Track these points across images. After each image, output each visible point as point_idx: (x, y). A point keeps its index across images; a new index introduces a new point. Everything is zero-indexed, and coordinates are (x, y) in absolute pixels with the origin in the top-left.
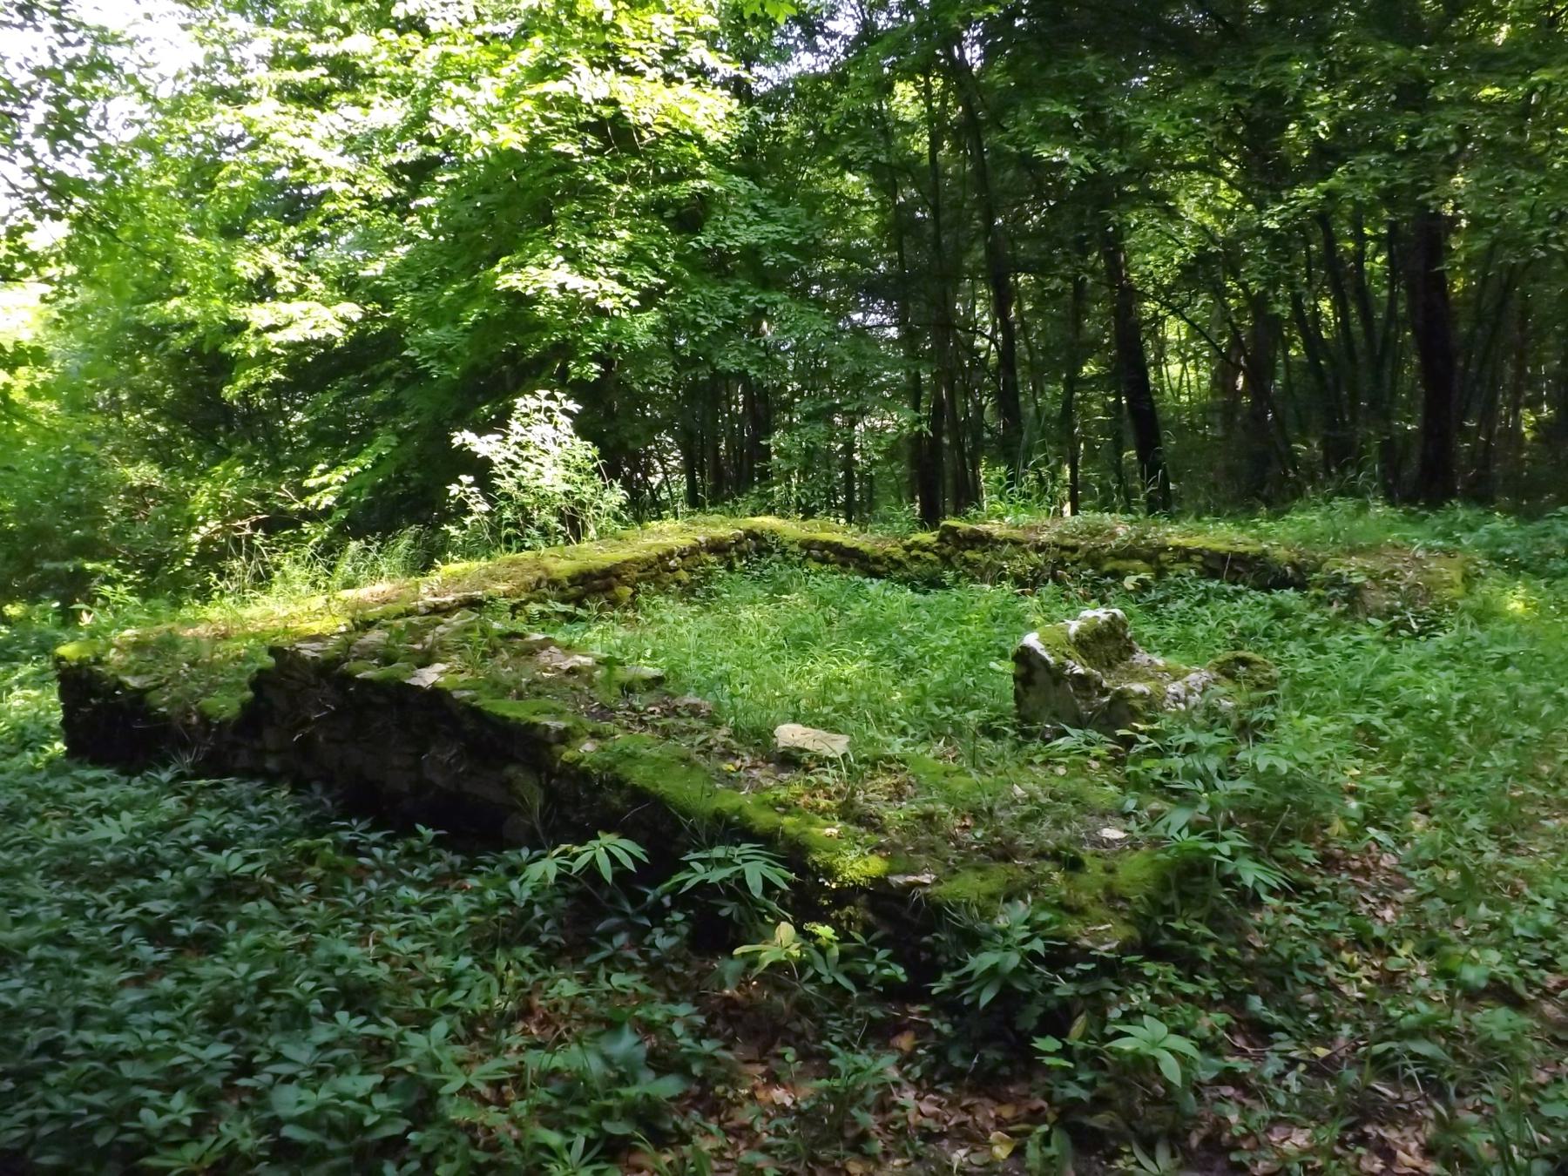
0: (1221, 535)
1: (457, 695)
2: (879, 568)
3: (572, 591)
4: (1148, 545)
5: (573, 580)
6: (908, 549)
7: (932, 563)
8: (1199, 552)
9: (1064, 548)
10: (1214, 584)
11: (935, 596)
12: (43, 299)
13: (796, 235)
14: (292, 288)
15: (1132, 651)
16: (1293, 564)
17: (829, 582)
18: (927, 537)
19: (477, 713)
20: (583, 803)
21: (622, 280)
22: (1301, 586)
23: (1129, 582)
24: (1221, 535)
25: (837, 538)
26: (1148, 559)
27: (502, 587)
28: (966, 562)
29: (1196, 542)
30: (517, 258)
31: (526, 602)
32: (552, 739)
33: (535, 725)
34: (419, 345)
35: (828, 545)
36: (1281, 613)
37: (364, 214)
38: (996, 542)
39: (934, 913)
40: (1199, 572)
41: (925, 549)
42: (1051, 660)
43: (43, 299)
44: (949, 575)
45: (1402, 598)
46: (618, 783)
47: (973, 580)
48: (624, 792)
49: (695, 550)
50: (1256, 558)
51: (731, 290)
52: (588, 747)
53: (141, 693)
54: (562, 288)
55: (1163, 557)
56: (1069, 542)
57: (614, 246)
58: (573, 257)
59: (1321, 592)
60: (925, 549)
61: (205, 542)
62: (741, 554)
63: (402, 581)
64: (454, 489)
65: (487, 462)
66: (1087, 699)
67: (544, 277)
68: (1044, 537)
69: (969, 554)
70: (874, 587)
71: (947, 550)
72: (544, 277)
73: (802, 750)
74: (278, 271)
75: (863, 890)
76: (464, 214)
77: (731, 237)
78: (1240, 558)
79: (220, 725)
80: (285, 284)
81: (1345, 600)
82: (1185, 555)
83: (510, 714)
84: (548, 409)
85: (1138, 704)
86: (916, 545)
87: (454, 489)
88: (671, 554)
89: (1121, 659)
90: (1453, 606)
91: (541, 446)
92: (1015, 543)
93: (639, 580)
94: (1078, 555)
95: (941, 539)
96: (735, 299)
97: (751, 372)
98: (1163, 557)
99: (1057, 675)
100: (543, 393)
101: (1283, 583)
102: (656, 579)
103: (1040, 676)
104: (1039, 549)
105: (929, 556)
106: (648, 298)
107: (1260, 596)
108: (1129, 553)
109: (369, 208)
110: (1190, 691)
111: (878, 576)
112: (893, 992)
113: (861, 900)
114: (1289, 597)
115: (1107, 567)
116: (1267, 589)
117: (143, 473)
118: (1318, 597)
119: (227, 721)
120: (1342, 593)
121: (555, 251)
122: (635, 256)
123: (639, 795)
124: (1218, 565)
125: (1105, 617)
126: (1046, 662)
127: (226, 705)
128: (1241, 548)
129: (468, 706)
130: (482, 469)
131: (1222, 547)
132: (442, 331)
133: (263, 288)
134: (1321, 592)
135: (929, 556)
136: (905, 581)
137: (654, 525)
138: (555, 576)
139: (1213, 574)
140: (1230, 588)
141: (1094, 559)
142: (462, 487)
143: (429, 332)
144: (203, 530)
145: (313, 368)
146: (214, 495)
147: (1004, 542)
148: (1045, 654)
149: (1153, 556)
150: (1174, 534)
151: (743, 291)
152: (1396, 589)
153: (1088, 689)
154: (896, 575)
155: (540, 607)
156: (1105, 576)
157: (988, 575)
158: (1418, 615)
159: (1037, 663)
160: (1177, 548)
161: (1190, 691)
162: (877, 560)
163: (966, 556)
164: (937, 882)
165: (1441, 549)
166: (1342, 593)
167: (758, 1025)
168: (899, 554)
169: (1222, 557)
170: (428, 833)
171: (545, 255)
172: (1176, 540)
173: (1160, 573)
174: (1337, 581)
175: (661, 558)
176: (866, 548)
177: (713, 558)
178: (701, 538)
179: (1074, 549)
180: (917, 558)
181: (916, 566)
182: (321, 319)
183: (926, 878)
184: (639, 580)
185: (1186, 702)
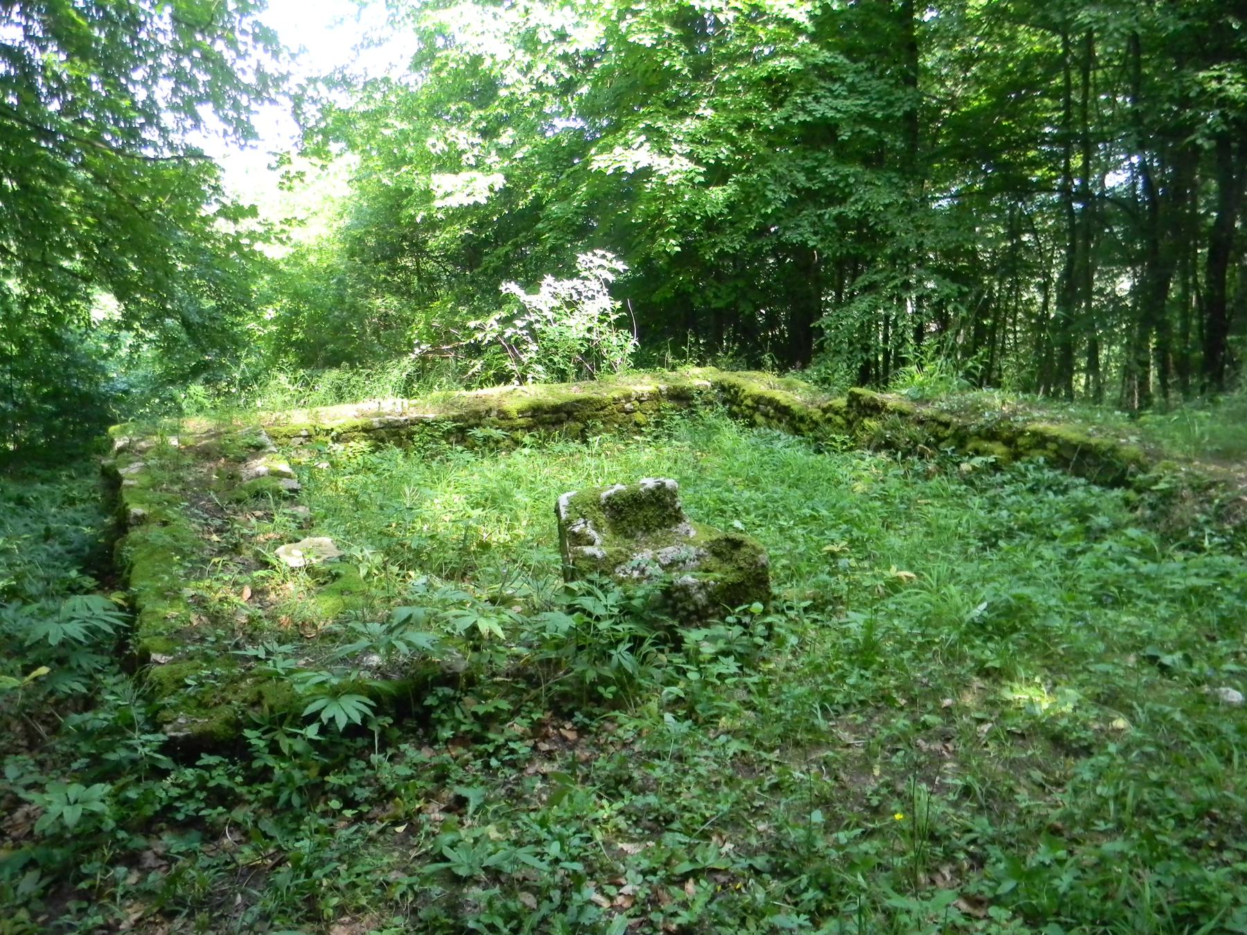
2: (803, 427)
3: (521, 421)
6: (825, 411)
8: (1055, 439)
12: (269, 167)
13: (883, 108)
14: (472, 161)
15: (678, 518)
26: (1009, 442)
31: (471, 427)
35: (771, 402)
38: (887, 411)
41: (837, 413)
43: (269, 167)
51: (809, 163)
56: (945, 417)
57: (697, 123)
69: (866, 422)
71: (851, 417)
81: (1152, 507)
82: (1041, 440)
88: (628, 398)
89: (660, 526)
92: (902, 414)
94: (949, 432)
96: (811, 173)
97: (811, 243)
100: (599, 252)
106: (717, 174)
111: (797, 431)
117: (384, 303)
135: (839, 420)
147: (893, 412)
148: (563, 510)
151: (821, 163)
160: (1034, 434)
162: (802, 419)
168: (817, 415)
176: (795, 408)
179: (947, 425)
180: (829, 420)
185: (643, 571)
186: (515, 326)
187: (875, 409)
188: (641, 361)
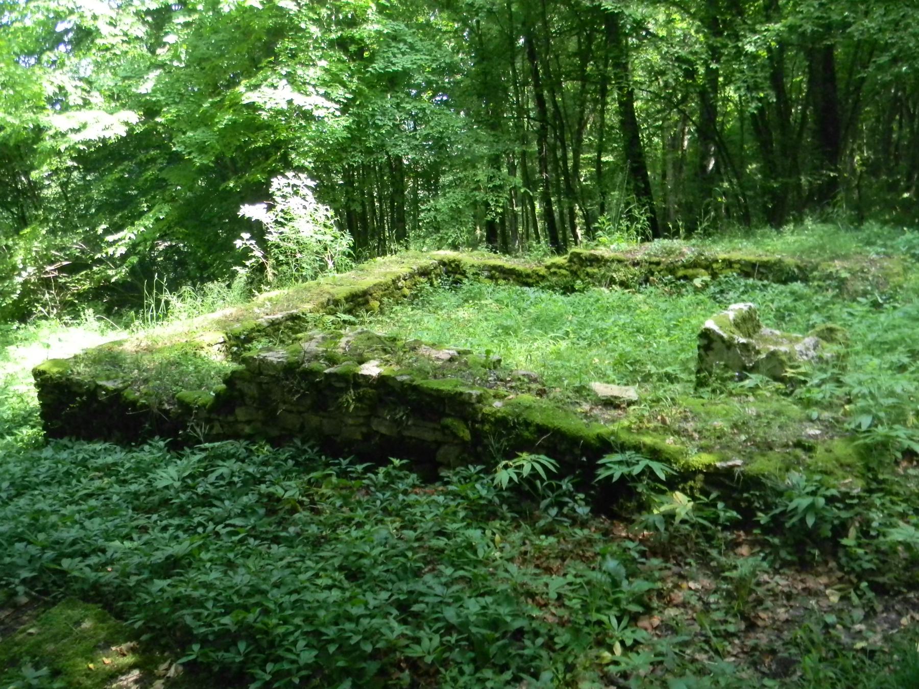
0: (744, 249)
1: (399, 379)
2: (530, 281)
4: (706, 259)
5: (346, 299)
6: (548, 268)
7: (565, 276)
8: (738, 262)
9: (651, 263)
10: (750, 281)
11: (572, 297)
16: (798, 267)
17: (506, 290)
18: (560, 260)
19: (415, 389)
20: (516, 434)
21: (326, 96)
22: (805, 280)
23: (697, 282)
24: (744, 249)
25: (498, 262)
26: (706, 268)
27: (308, 307)
28: (587, 274)
29: (735, 256)
30: (253, 81)
32: (474, 401)
33: (461, 393)
34: (183, 143)
35: (494, 268)
36: (797, 297)
37: (125, 47)
38: (607, 261)
39: (754, 482)
40: (739, 274)
42: (725, 336)
44: (578, 284)
45: (871, 285)
46: (527, 424)
47: (594, 285)
48: (532, 429)
49: (412, 275)
50: (775, 264)
52: (497, 404)
53: (117, 393)
54: (290, 102)
55: (715, 266)
56: (655, 259)
58: (291, 78)
59: (821, 283)
60: (559, 267)
61: (26, 282)
62: (438, 275)
63: (240, 305)
64: (238, 243)
65: (259, 223)
66: (748, 356)
67: (271, 95)
68: (639, 257)
69: (589, 270)
70: (531, 293)
71: (575, 268)
72: (271, 95)
73: (616, 397)
74: (69, 88)
75: (701, 472)
76: (203, 49)
77: (394, 64)
78: (765, 265)
79: (199, 408)
80: (74, 98)
81: (837, 287)
82: (729, 264)
83: (442, 388)
84: (294, 186)
85: (784, 358)
86: (553, 265)
87: (238, 243)
88: (399, 278)
89: (755, 332)
90: (901, 287)
91: (298, 212)
92: (620, 261)
93: (383, 296)
94: (661, 267)
95: (570, 261)
98: (715, 266)
99: (729, 345)
101: (794, 279)
102: (391, 295)
103: (717, 345)
104: (636, 264)
105: (564, 272)
107: (782, 287)
108: (695, 265)
109: (129, 43)
110: (808, 349)
111: (529, 285)
112: (733, 525)
113: (701, 477)
114: (797, 286)
115: (681, 273)
116: (785, 282)
118: (819, 286)
119: (204, 405)
120: (835, 283)
121: (282, 76)
122: (335, 79)
123: (541, 430)
124: (749, 270)
125: (746, 309)
126: (721, 337)
127: (207, 396)
128: (765, 259)
129: (410, 385)
130: (258, 230)
131: (752, 258)
132: (199, 131)
133: (59, 101)
134: (821, 283)
135: (564, 272)
136: (551, 287)
137: (379, 259)
138: (337, 297)
139: (747, 275)
140: (760, 283)
141: (672, 270)
142: (244, 240)
143: (190, 134)
144: (24, 274)
145: (97, 157)
146: (28, 251)
147: (613, 261)
148: (721, 333)
149: (708, 266)
150: (720, 250)
152: (867, 280)
153: (749, 351)
154: (542, 284)
155: (332, 318)
156: (679, 279)
157: (603, 282)
158: (882, 293)
159: (715, 338)
160: (724, 261)
161: (808, 349)
162: (528, 276)
163: (581, 274)
164: (745, 464)
165: (885, 253)
166: (835, 283)
167: (670, 546)
168: (543, 271)
169: (753, 265)
170: (397, 462)
171: (274, 79)
172: (722, 256)
173: (714, 275)
174: (829, 276)
175: (394, 282)
176: (520, 268)
177: (422, 279)
178: (415, 267)
179: (658, 264)
180: (555, 273)
181: (554, 279)
182: (109, 124)
183: (738, 462)
184: (383, 296)
186: (242, 239)
187: (595, 260)
188: (358, 253)
